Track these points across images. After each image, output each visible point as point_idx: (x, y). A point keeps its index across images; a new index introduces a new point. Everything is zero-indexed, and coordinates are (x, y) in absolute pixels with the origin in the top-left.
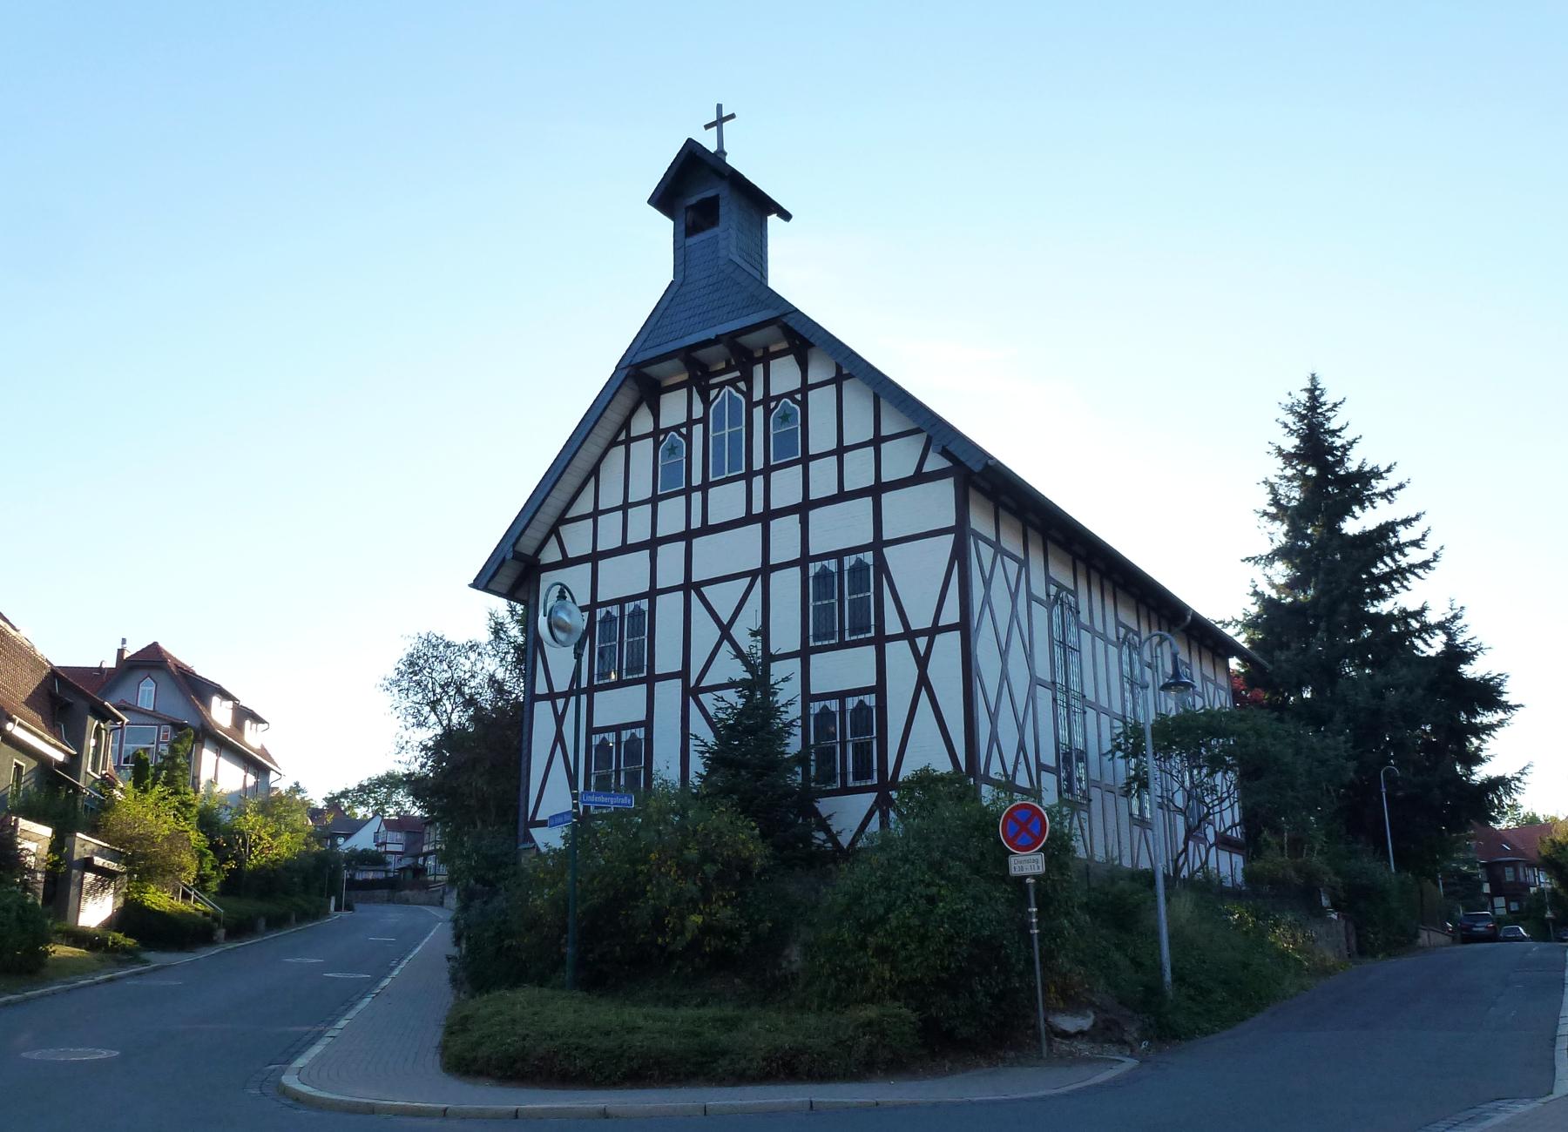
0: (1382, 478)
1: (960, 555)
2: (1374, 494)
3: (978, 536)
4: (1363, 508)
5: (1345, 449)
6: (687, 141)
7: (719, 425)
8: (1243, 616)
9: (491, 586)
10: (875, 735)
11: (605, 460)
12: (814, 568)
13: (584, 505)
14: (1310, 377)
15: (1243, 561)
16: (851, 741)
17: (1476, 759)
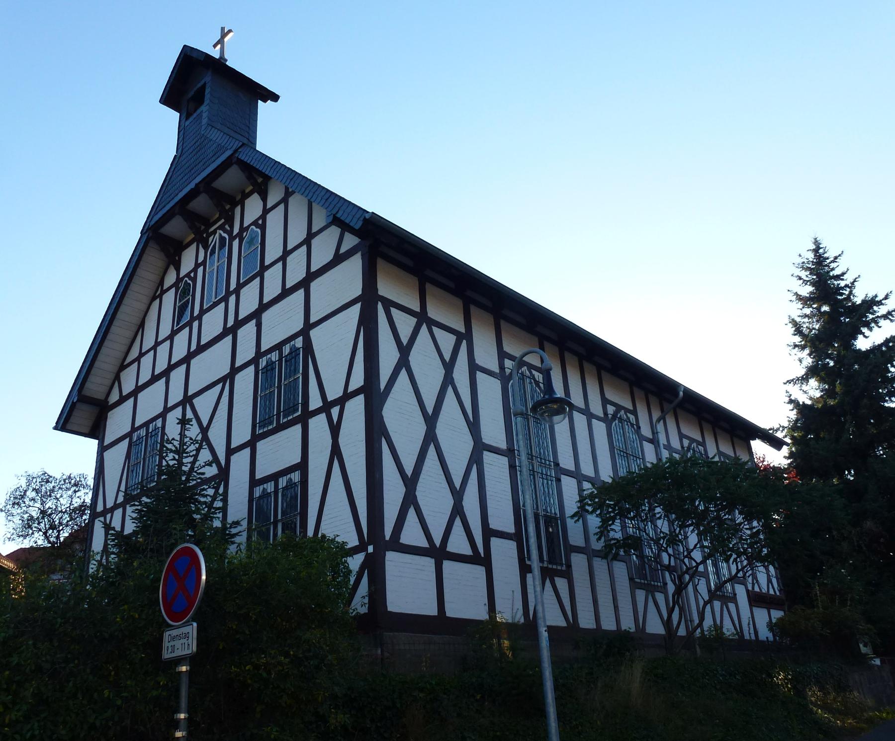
0: (882, 304)
1: (367, 323)
2: (878, 317)
3: (389, 304)
4: (871, 329)
5: (851, 287)
7: (212, 264)
8: (788, 423)
9: (69, 427)
11: (148, 314)
12: (263, 362)
13: (134, 353)
14: (813, 241)
15: (785, 383)
17: (811, 293)
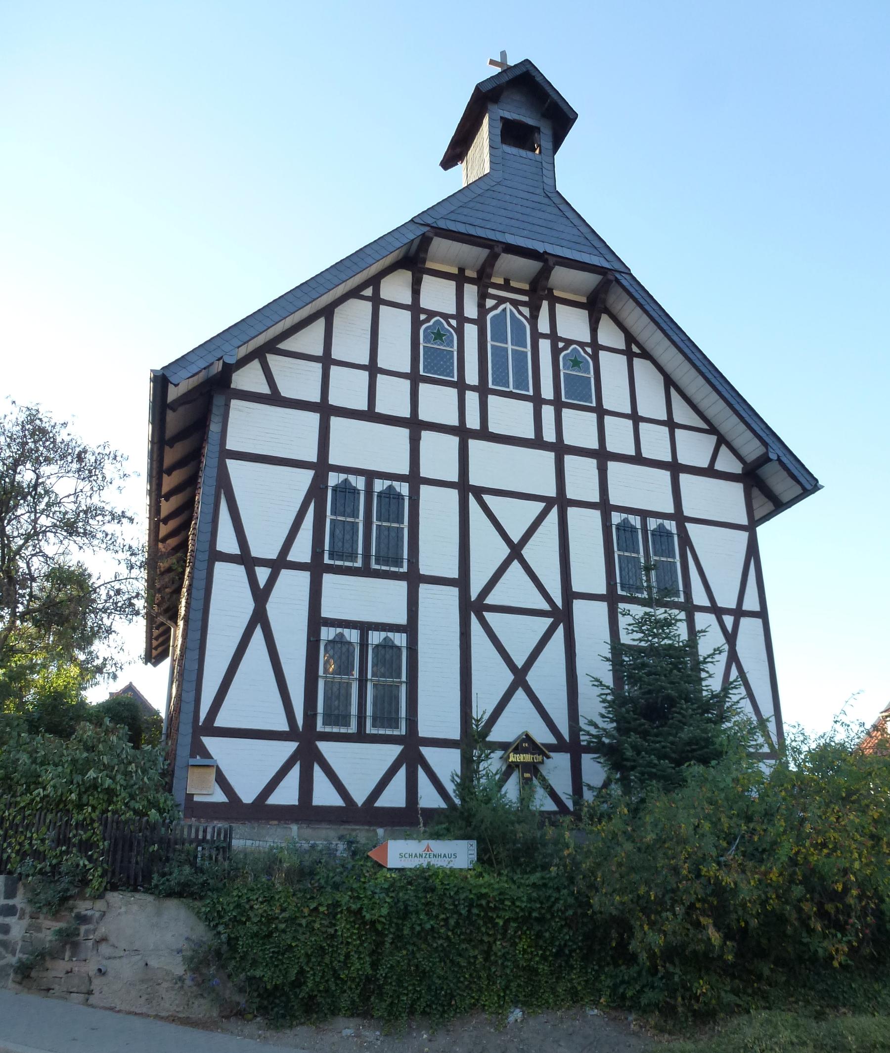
6: (525, 61)
10: (404, 678)
13: (682, 414)
16: (371, 680)
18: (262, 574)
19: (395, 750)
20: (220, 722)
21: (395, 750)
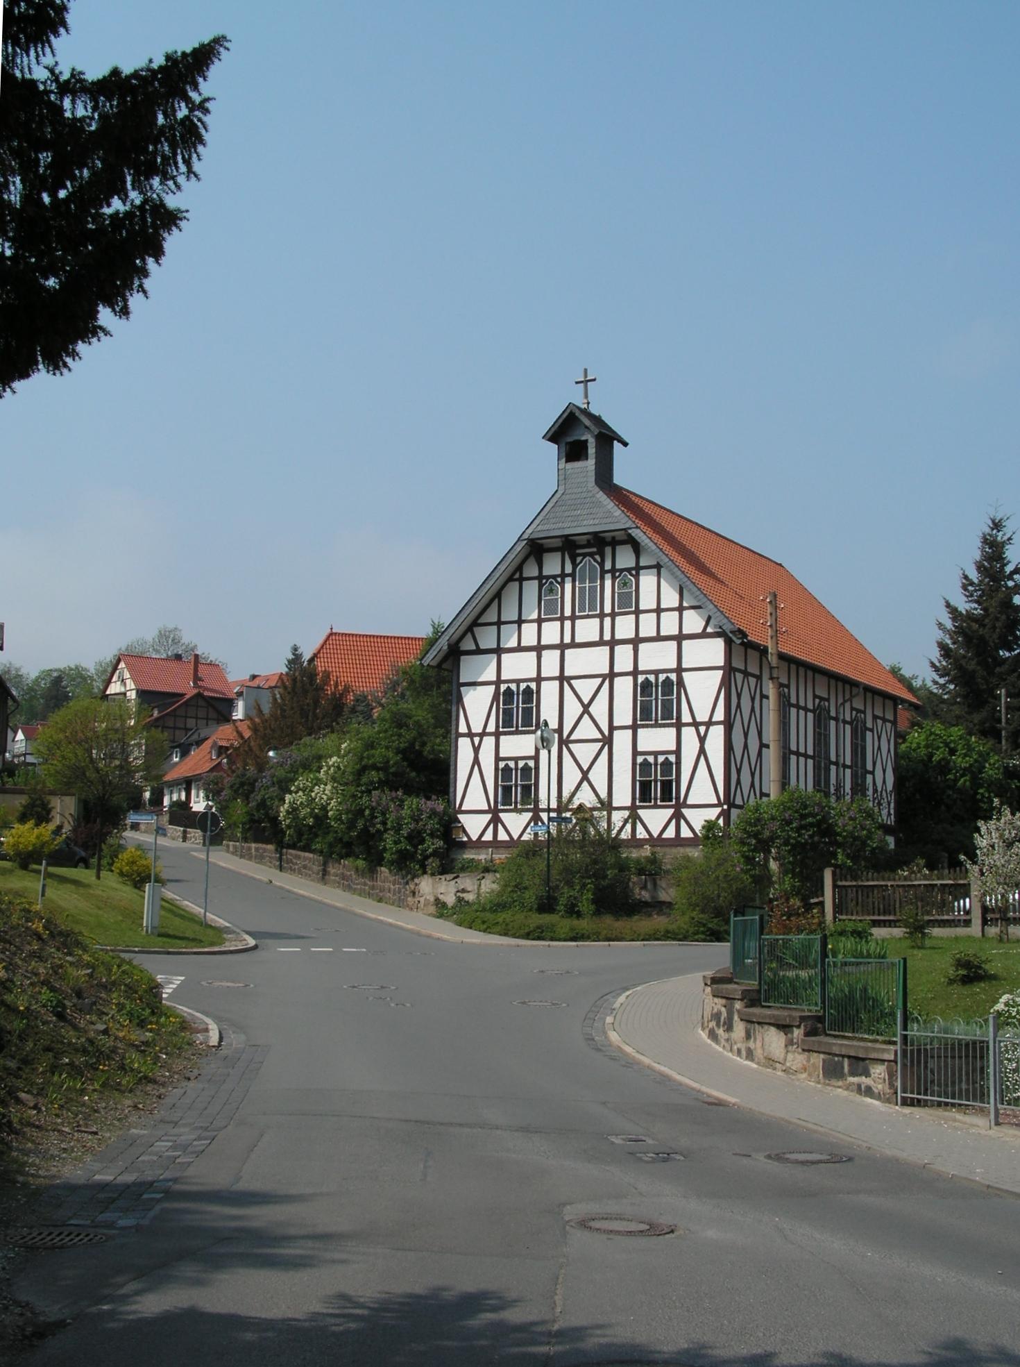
13: (491, 616)
18: (477, 740)
19: (530, 814)
20: (689, 802)
21: (530, 814)
